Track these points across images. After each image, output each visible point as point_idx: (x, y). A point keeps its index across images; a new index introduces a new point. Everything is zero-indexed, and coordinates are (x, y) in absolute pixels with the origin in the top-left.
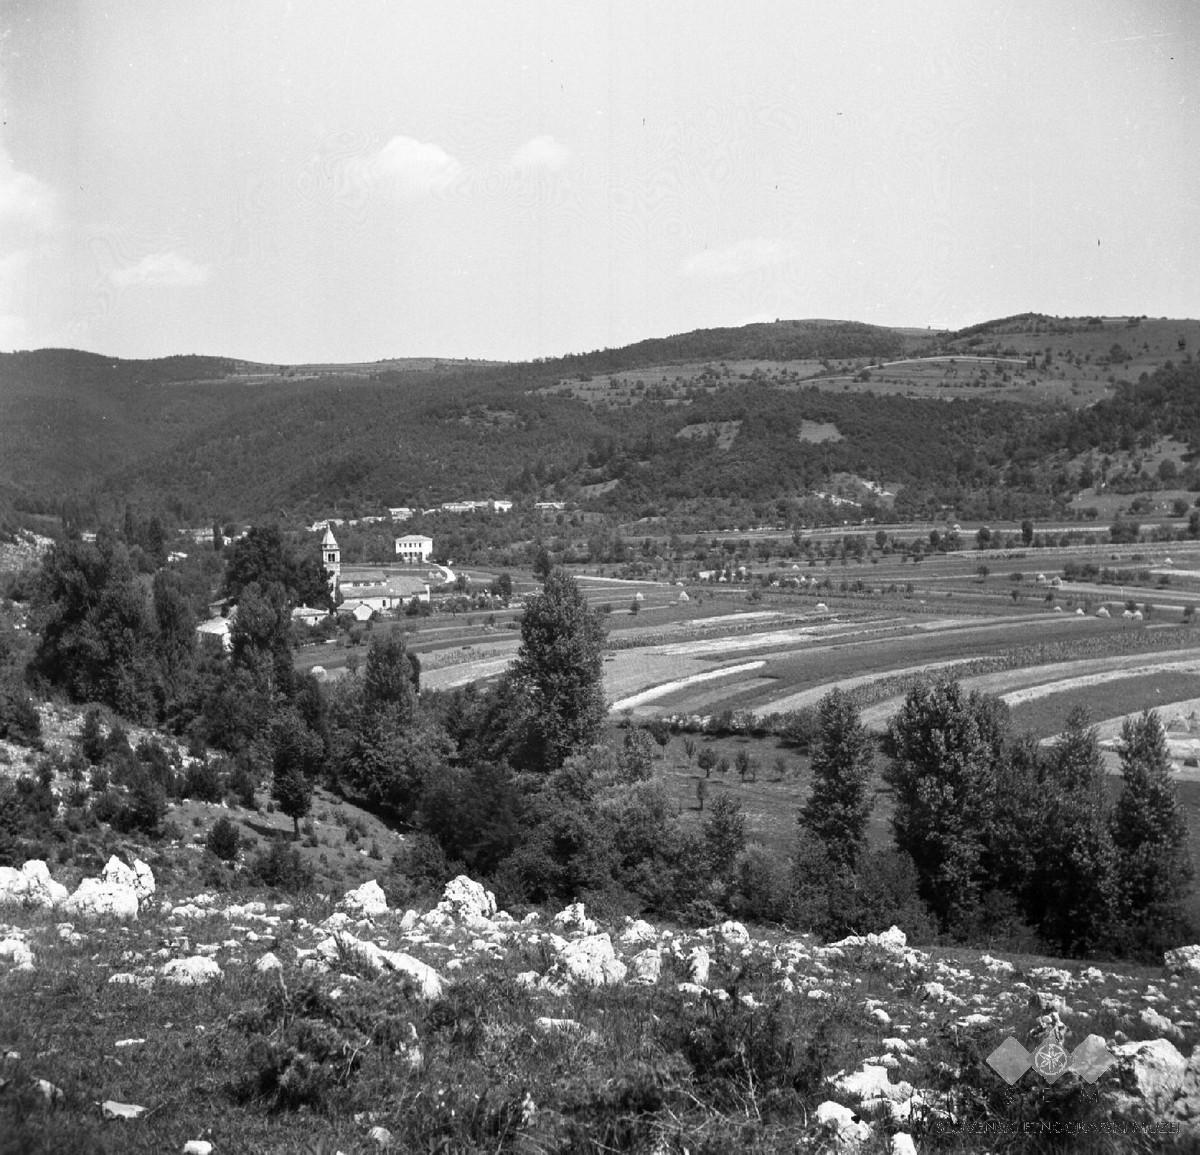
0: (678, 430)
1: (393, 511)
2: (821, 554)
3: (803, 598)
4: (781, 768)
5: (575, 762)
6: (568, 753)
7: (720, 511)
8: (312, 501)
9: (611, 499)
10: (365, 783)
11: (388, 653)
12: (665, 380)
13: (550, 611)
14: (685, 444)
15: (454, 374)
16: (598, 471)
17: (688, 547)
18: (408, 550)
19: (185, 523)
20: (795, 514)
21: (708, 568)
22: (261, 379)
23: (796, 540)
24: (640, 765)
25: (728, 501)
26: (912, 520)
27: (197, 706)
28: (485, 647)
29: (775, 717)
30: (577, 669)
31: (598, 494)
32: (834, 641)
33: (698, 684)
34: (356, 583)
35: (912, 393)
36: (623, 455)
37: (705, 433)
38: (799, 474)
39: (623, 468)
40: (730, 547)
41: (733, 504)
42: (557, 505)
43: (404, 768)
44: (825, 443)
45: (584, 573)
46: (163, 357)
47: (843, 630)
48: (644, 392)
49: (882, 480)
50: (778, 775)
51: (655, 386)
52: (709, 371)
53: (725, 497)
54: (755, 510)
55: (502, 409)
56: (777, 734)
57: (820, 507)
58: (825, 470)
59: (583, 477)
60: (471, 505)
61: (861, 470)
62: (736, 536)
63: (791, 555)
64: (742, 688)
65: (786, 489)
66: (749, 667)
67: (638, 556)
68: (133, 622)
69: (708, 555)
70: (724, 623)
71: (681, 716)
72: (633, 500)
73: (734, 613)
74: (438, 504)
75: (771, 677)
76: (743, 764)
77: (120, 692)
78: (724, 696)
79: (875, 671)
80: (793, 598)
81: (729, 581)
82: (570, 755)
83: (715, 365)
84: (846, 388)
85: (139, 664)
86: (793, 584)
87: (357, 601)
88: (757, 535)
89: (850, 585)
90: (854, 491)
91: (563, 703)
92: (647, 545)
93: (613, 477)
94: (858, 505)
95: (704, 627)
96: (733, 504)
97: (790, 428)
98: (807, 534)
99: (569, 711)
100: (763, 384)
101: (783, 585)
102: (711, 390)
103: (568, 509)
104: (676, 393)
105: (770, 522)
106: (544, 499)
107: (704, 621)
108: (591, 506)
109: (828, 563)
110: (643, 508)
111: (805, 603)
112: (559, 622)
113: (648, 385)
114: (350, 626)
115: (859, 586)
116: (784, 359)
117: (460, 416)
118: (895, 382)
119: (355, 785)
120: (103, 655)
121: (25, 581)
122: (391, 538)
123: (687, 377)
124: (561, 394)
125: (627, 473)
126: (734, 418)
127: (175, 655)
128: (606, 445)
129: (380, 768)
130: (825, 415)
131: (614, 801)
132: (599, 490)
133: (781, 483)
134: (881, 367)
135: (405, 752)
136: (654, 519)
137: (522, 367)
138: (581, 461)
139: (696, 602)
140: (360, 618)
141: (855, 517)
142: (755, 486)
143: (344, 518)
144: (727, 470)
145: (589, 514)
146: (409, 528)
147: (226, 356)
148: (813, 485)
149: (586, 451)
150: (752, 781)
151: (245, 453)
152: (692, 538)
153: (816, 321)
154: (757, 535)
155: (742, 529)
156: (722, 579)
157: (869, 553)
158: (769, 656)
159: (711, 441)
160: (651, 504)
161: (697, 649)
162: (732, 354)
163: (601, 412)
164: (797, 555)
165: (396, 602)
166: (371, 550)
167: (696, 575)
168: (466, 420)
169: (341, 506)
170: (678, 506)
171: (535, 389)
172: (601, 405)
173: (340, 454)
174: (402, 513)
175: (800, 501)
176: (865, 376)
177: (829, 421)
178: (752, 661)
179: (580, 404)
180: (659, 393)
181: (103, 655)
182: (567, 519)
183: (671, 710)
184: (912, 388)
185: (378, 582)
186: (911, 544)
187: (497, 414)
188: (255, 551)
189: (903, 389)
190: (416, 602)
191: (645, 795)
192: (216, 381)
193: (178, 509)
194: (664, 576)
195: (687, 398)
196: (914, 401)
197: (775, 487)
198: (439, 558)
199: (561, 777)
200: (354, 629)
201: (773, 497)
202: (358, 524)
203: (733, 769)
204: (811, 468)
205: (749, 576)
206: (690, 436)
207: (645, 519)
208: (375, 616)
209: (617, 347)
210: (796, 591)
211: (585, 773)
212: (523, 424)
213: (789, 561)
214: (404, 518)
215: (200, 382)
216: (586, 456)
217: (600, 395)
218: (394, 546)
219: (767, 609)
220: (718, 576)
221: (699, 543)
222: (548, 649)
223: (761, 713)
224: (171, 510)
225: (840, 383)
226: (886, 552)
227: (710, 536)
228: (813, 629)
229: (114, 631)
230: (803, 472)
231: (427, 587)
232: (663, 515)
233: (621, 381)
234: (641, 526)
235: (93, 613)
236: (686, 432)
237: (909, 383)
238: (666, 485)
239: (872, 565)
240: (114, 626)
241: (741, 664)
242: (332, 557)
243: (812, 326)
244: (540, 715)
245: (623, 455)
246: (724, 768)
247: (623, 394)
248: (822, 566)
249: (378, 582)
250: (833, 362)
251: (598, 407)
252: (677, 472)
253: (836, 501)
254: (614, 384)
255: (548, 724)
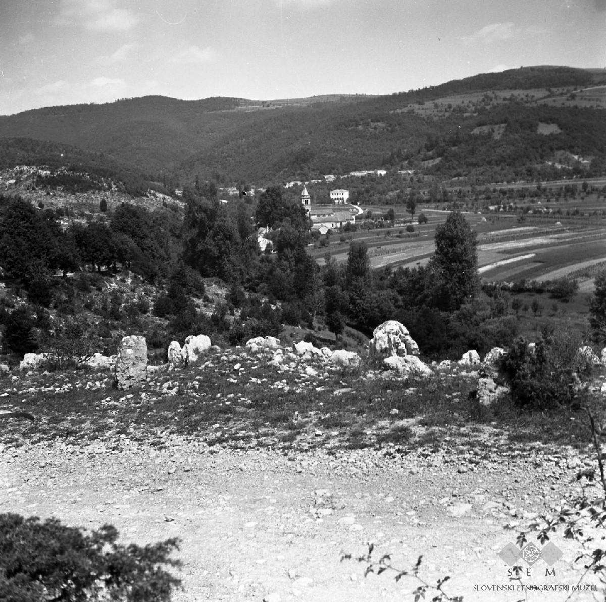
0: (472, 130)
1: (326, 177)
2: (553, 195)
3: (547, 220)
4: (555, 309)
5: (466, 306)
6: (462, 302)
7: (495, 173)
8: (285, 172)
9: (438, 168)
10: (357, 316)
11: (359, 252)
12: (463, 102)
13: (451, 230)
14: (476, 138)
15: (352, 103)
16: (431, 153)
17: (481, 193)
18: (336, 197)
19: (222, 185)
20: (536, 174)
21: (493, 204)
22: (253, 109)
23: (539, 188)
24: (503, 309)
25: (500, 168)
26: (601, 176)
27: (260, 278)
28: (388, 247)
29: (548, 283)
30: (465, 260)
31: (430, 165)
32: (569, 243)
33: (502, 265)
34: (318, 215)
35: (599, 106)
36: (443, 144)
37: (486, 131)
38: (537, 152)
39: (444, 151)
40: (503, 192)
41: (502, 169)
42: (409, 172)
43: (377, 309)
44: (552, 134)
45: (428, 208)
46: (141, 97)
47: (573, 236)
48: (452, 109)
49: (583, 154)
50: (553, 312)
51: (458, 106)
52: (487, 97)
53: (498, 165)
54: (514, 172)
55: (378, 121)
56: (549, 291)
57: (549, 169)
58: (552, 150)
59: (422, 156)
60: (365, 173)
61: (571, 149)
62: (505, 186)
63: (536, 196)
64: (526, 268)
65: (531, 160)
66: (527, 256)
67: (455, 198)
68: (229, 237)
69: (492, 197)
70: (508, 233)
71: (497, 283)
72: (449, 168)
73: (512, 228)
74: (348, 172)
75: (540, 262)
76: (536, 307)
77: (225, 272)
78: (517, 272)
79: (595, 258)
80: (543, 220)
81: (505, 211)
82: (464, 303)
83: (490, 93)
84: (563, 104)
85: (233, 258)
86: (540, 212)
87: (319, 224)
88: (519, 185)
89: (571, 212)
90: (567, 160)
91: (459, 278)
92: (460, 192)
93: (438, 156)
94: (570, 168)
95: (497, 235)
96: (502, 169)
97: (532, 127)
98: (544, 184)
99: (461, 282)
100: (517, 103)
101: (535, 212)
102: (488, 107)
103: (415, 173)
104: (469, 110)
105: (523, 179)
106: (402, 168)
107: (498, 232)
108: (428, 171)
109: (557, 200)
110: (454, 172)
111: (549, 222)
112: (457, 237)
113: (454, 106)
114: (319, 237)
115: (577, 212)
116: (526, 89)
117: (357, 125)
118: (590, 100)
119: (351, 317)
120: (217, 253)
121: (158, 216)
122: (327, 191)
123: (474, 100)
124: (409, 112)
125: (446, 154)
126: (502, 123)
127: (249, 253)
128: (434, 139)
129: (363, 309)
130: (551, 120)
131: (492, 326)
132: (430, 163)
133: (528, 157)
134: (581, 91)
135: (377, 301)
136: (460, 178)
137: (387, 98)
138: (421, 148)
139: (491, 222)
140: (322, 233)
141: (569, 174)
142: (514, 159)
143: (302, 181)
144: (499, 151)
145: (426, 177)
146: (336, 185)
147: (235, 97)
148: (545, 157)
149: (424, 142)
150: (540, 316)
151: (248, 148)
152: (483, 188)
153: (543, 66)
154: (519, 185)
155: (508, 182)
156: (502, 209)
157: (579, 194)
158: (536, 251)
159: (490, 135)
160: (459, 170)
161: (497, 248)
162: (498, 87)
163: (429, 121)
164: (540, 196)
165: (339, 225)
166: (318, 198)
167: (487, 208)
168: (360, 128)
169: (299, 175)
170: (474, 171)
171: (395, 109)
172: (430, 117)
173: (297, 147)
174: (331, 178)
175: (538, 167)
176: (573, 97)
177: (553, 123)
178: (528, 254)
179: (418, 117)
180: (460, 110)
181: (217, 253)
182: (415, 179)
183: (491, 279)
184: (599, 103)
185: (329, 215)
186: (602, 189)
187: (376, 124)
188: (269, 199)
189: (594, 103)
190: (349, 224)
191: (507, 323)
192: (231, 111)
193: (218, 177)
194: (471, 208)
195: (474, 112)
196: (600, 110)
197: (525, 159)
198: (353, 200)
199: (459, 314)
200: (321, 238)
201: (524, 165)
202: (309, 184)
203: (530, 310)
204: (545, 148)
205: (516, 208)
206: (478, 133)
207: (456, 178)
208: (329, 231)
209: (437, 85)
210: (542, 215)
211: (471, 312)
212: (389, 128)
213: (535, 199)
214: (331, 180)
215: (224, 111)
216: (423, 145)
217: (428, 112)
218: (329, 195)
219: (529, 226)
220: (499, 208)
221: (487, 190)
222: (451, 250)
223: (541, 279)
224: (213, 178)
225: (558, 102)
226: (588, 193)
227: (492, 186)
228: (556, 236)
229: (221, 242)
230: (540, 151)
231: (354, 217)
232: (466, 175)
233: (440, 104)
234: (455, 182)
235: (211, 233)
236: (476, 131)
237: (597, 100)
238: (467, 159)
239: (581, 201)
240: (221, 240)
241: (523, 255)
242: (306, 202)
243: (541, 69)
244: (447, 283)
245: (443, 144)
246: (526, 309)
247: (441, 111)
248: (554, 202)
249: (329, 215)
250: (554, 90)
251: (428, 118)
252: (472, 152)
253: (559, 166)
254: (436, 106)
255: (452, 288)
